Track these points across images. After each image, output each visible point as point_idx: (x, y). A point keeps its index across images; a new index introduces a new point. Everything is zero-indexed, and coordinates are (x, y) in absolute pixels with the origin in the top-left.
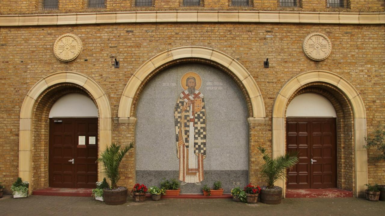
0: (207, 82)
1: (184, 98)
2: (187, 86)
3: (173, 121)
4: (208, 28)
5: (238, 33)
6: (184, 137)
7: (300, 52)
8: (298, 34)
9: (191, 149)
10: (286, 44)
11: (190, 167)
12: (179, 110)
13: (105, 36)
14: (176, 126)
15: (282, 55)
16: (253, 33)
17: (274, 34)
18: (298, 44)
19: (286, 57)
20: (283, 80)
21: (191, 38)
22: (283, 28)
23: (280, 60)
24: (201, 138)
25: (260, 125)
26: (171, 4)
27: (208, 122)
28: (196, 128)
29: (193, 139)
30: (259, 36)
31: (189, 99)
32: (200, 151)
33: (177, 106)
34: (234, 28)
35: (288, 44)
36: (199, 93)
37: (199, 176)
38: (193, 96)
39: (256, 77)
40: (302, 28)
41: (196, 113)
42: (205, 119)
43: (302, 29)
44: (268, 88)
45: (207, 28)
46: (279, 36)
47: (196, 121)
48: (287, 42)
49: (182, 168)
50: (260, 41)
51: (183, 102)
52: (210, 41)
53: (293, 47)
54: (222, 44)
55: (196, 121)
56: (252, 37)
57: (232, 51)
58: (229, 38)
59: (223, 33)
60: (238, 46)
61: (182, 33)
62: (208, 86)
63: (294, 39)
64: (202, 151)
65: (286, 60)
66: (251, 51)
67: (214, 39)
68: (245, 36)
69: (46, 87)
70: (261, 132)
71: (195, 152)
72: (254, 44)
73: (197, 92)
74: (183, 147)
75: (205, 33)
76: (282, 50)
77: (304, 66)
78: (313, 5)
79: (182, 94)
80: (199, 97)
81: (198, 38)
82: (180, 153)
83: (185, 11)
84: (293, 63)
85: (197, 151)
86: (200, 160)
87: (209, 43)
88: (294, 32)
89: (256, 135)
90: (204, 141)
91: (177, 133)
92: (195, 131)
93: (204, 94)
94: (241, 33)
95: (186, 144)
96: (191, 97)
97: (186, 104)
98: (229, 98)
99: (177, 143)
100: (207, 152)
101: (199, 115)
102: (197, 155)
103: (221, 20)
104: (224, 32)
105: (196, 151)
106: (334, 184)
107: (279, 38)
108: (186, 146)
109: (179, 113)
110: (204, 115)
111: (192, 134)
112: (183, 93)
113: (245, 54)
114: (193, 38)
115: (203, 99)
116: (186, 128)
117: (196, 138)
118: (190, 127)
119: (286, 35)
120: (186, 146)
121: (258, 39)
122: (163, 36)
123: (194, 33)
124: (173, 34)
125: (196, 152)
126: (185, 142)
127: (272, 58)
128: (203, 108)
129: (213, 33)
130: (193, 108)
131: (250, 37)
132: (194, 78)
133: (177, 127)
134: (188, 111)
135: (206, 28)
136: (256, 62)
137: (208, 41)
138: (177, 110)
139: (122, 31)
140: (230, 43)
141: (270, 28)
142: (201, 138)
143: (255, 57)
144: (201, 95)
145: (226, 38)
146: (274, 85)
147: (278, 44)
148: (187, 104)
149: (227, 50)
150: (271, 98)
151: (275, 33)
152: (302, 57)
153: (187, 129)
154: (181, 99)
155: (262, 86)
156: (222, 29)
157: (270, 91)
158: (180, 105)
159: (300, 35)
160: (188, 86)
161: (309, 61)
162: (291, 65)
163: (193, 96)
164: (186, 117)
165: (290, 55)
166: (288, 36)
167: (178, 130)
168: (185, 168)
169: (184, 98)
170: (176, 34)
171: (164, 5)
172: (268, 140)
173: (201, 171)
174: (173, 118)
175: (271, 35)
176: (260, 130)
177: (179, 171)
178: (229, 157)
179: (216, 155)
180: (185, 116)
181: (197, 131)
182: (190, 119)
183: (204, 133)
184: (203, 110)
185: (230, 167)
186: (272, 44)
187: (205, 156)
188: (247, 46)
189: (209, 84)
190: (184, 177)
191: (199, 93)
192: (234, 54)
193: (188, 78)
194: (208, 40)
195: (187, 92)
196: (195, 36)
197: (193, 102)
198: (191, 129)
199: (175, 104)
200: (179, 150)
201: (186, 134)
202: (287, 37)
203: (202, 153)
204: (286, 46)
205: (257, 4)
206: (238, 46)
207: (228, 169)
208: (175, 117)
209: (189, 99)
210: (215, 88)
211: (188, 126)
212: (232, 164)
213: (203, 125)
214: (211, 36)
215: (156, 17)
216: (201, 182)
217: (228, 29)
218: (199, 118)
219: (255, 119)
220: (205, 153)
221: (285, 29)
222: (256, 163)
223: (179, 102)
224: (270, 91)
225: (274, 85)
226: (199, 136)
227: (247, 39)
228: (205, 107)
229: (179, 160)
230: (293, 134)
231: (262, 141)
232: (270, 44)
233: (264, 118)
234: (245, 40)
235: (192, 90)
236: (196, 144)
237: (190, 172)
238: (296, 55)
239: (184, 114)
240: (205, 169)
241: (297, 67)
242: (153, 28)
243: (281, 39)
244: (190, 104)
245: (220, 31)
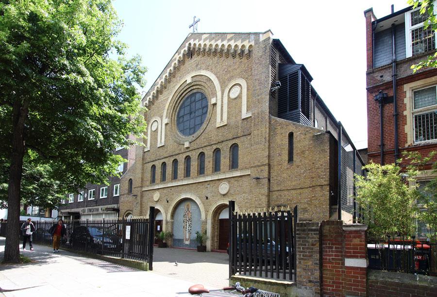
4: (191, 185)
13: (165, 191)
33: (184, 216)
39: (204, 204)
83: (161, 184)
84: (216, 196)
94: (201, 187)
106: (206, 251)
139: (169, 189)
215: (225, 176)
218: (190, 220)
230: (271, 230)
235: (188, 209)
237: (187, 240)
242: (176, 188)
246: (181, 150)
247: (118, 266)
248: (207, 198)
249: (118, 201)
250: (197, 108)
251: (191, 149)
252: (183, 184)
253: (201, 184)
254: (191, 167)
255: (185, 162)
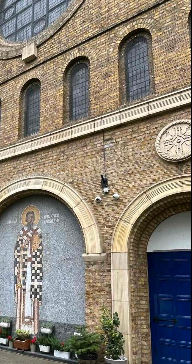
0: (45, 215)
1: (23, 235)
2: (26, 221)
3: (12, 260)
5: (72, 152)
6: (22, 278)
7: (151, 156)
8: (148, 132)
9: (28, 294)
10: (131, 150)
11: (26, 315)
12: (18, 249)
14: (15, 266)
15: (126, 165)
16: (89, 148)
17: (114, 141)
18: (149, 146)
19: (132, 167)
20: (127, 200)
21: (26, 170)
22: (127, 129)
23: (122, 173)
24: (38, 280)
25: (95, 263)
26: (11, 139)
27: (44, 262)
28: (33, 269)
29: (30, 281)
30: (96, 149)
31: (27, 236)
32: (36, 297)
33: (18, 245)
34: (68, 148)
35: (133, 148)
36: (37, 229)
37: (34, 326)
38: (31, 232)
40: (154, 121)
41: (34, 251)
42: (42, 258)
43: (154, 123)
44: (106, 214)
45: (42, 154)
46: (121, 142)
47: (33, 261)
48: (132, 146)
49: (19, 315)
50: (96, 155)
51: (23, 239)
52: (44, 168)
53: (142, 151)
54: (55, 168)
55: (33, 261)
56: (87, 153)
57: (64, 175)
58: (62, 161)
59: (56, 157)
60: (71, 167)
61: (18, 167)
62: (46, 219)
63: (143, 140)
64: (38, 296)
65: (131, 172)
66: (87, 170)
67: (47, 165)
68: (80, 153)
69: (129, 227)
70: (97, 274)
71: (31, 297)
72: (90, 160)
73: (35, 228)
74: (21, 290)
75: (39, 162)
76: (126, 158)
77: (159, 174)
78: (172, 83)
79: (22, 231)
80: (37, 233)
81: (32, 168)
82: (17, 298)
85: (33, 296)
86: (36, 307)
87: (42, 171)
88: (143, 130)
89: (91, 278)
90: (40, 284)
91: (16, 275)
92: (32, 272)
93: (41, 229)
94: (78, 152)
95: (24, 287)
96: (29, 234)
97: (25, 241)
98: (67, 231)
99: (16, 285)
100: (43, 297)
101: (36, 253)
102: (33, 300)
103: (54, 142)
104: (57, 155)
105: (32, 295)
107: (122, 144)
108: (23, 289)
109: (18, 252)
110: (40, 254)
111: (29, 275)
112: (23, 230)
113: (79, 174)
114: (28, 170)
115: (40, 235)
116: (24, 268)
117: (32, 281)
118: (28, 267)
119: (130, 137)
120: (23, 289)
121: (94, 153)
122: (4, 173)
123: (29, 164)
124: (12, 169)
125: (32, 297)
126: (22, 284)
127: (112, 173)
128: (41, 245)
129: (46, 159)
130: (31, 245)
131: (85, 153)
132: (33, 212)
133: (16, 268)
134: (26, 250)
135: (40, 156)
136: (91, 182)
137: (42, 169)
138: (16, 249)
140: (63, 166)
141: (109, 135)
142: (38, 280)
143: (91, 175)
144: (39, 231)
145: (60, 161)
146: (114, 208)
147: (120, 153)
148: (26, 242)
149: (60, 174)
150: (110, 226)
151: (116, 139)
152: (155, 162)
153: (25, 269)
154: (20, 236)
155: (99, 212)
156: (54, 154)
157: (109, 216)
158: (20, 243)
159: (151, 131)
160: (28, 222)
161: (166, 165)
162: (138, 177)
163: (31, 232)
164: (25, 255)
165: (136, 163)
166: (134, 137)
167: (16, 271)
168: (22, 315)
169: (23, 235)
170: (15, 168)
171: (6, 142)
172: (107, 285)
173: (36, 321)
174: (13, 258)
175: (111, 143)
176: (96, 270)
177: (16, 318)
178: (66, 305)
179: (52, 302)
180: (23, 254)
181: (34, 272)
182: (28, 258)
183: (41, 275)
184: (41, 247)
185: (67, 320)
186: (112, 155)
187: (40, 302)
188: (81, 165)
189: (47, 216)
190: (20, 326)
191: (37, 229)
192: (67, 178)
193: (28, 213)
194: (41, 167)
195: (26, 229)
196: (30, 166)
197: (31, 239)
198: (29, 270)
199: (15, 242)
200: (17, 293)
201: (24, 275)
202: (131, 140)
203: (38, 299)
204: (131, 152)
205: (94, 111)
206: (71, 167)
207: (65, 322)
208: (15, 256)
209: (27, 236)
210: (53, 221)
211: (26, 267)
212: (69, 316)
213: (40, 265)
214: (44, 163)
216: (36, 335)
217: (62, 150)
218: (36, 256)
219: (89, 255)
220: (40, 299)
221: (130, 130)
222: (91, 316)
223: (18, 241)
224: (109, 216)
225: (114, 208)
226: (36, 278)
227: (82, 157)
228: (42, 244)
229: (16, 305)
231: (99, 285)
232: (110, 155)
233: (100, 253)
234: (79, 158)
236: (32, 287)
238: (145, 161)
239: (23, 252)
240: (40, 319)
241: (148, 178)
243: (124, 145)
244: (29, 241)
245: (53, 155)
246: (10, 71)
247: (3, 350)
248: (104, 183)
249: (31, 287)
250: (86, 85)
251: (41, 59)
252: (17, 153)
253: (79, 144)
254: (43, 105)
255: (21, 99)
